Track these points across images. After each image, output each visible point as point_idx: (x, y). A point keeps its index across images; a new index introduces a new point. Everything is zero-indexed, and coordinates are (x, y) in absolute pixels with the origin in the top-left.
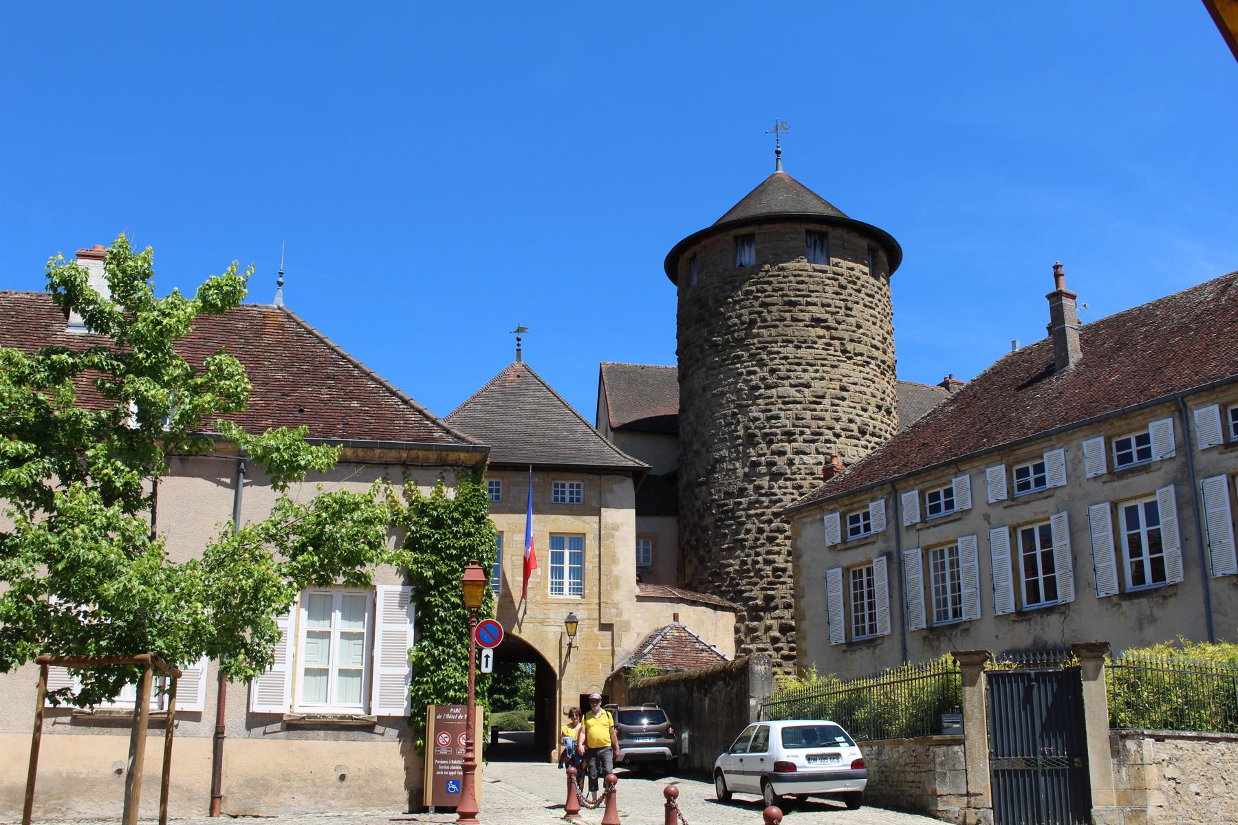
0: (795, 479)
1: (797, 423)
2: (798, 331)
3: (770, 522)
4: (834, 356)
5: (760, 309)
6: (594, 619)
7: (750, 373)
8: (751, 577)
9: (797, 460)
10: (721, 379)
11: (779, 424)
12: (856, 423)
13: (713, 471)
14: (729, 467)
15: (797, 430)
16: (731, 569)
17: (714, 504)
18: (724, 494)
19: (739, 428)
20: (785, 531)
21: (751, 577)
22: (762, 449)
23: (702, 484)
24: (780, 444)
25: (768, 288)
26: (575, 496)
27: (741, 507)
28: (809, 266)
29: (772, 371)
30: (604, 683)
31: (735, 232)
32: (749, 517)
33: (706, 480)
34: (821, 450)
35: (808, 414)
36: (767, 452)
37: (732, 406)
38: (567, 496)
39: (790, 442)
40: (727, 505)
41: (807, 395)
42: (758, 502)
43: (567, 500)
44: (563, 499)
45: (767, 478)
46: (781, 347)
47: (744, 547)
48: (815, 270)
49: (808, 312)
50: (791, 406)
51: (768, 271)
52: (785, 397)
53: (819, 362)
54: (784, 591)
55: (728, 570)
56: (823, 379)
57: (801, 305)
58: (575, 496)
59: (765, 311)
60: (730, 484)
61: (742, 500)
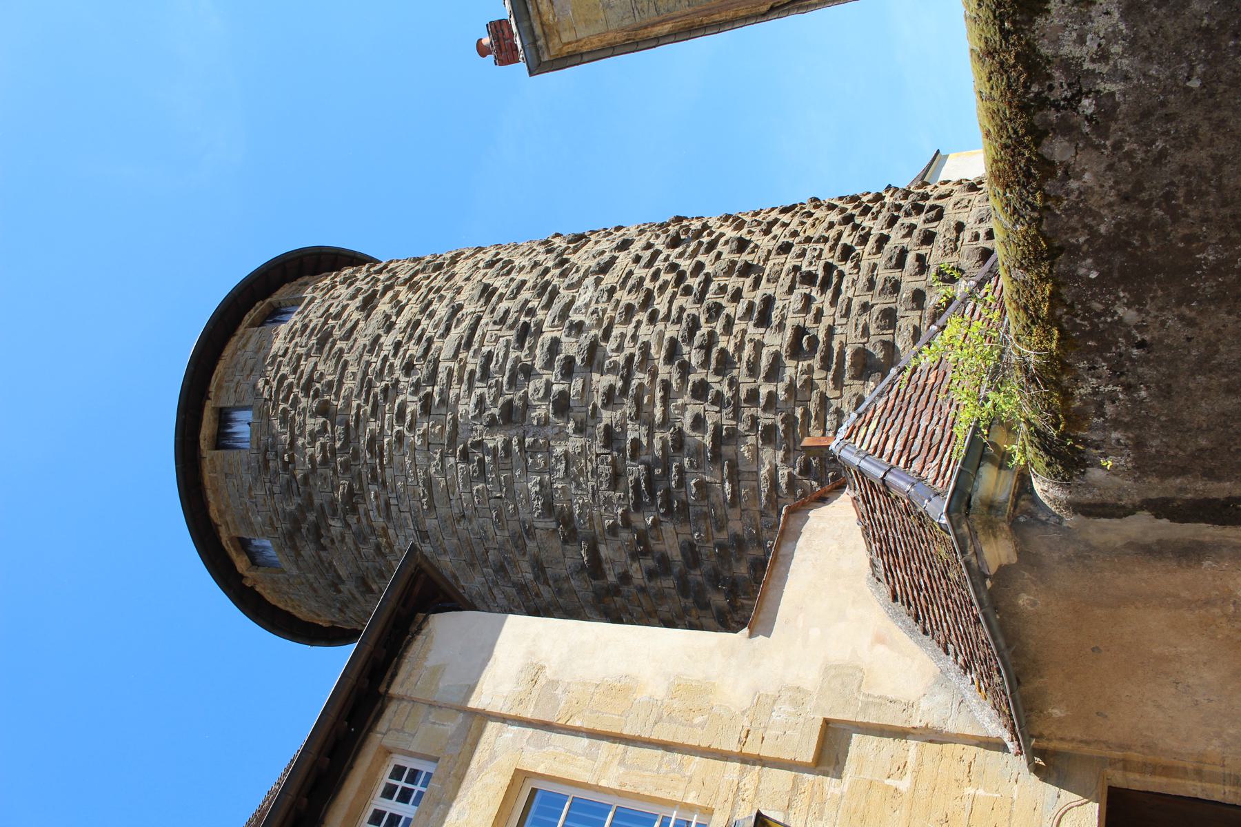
0: (612, 319)
1: (509, 321)
3: (685, 369)
4: (435, 278)
5: (312, 393)
6: (795, 787)
7: (401, 416)
8: (806, 413)
9: (575, 317)
10: (405, 486)
11: (501, 354)
13: (566, 519)
14: (561, 474)
16: (783, 472)
17: (635, 518)
18: (615, 490)
19: (491, 445)
20: (712, 334)
21: (806, 413)
22: (537, 390)
23: (593, 552)
24: (538, 352)
25: (291, 379)
27: (644, 441)
28: (294, 318)
29: (409, 368)
30: (1051, 789)
32: (666, 422)
33: (586, 540)
35: (504, 305)
36: (545, 377)
37: (452, 460)
39: (539, 332)
40: (637, 481)
41: (473, 310)
42: (638, 400)
45: (596, 376)
46: (378, 355)
47: (733, 433)
48: (302, 312)
50: (479, 332)
51: (267, 382)
52: (459, 344)
54: (850, 330)
55: (783, 482)
57: (333, 327)
59: (318, 385)
60: (594, 472)
61: (631, 435)
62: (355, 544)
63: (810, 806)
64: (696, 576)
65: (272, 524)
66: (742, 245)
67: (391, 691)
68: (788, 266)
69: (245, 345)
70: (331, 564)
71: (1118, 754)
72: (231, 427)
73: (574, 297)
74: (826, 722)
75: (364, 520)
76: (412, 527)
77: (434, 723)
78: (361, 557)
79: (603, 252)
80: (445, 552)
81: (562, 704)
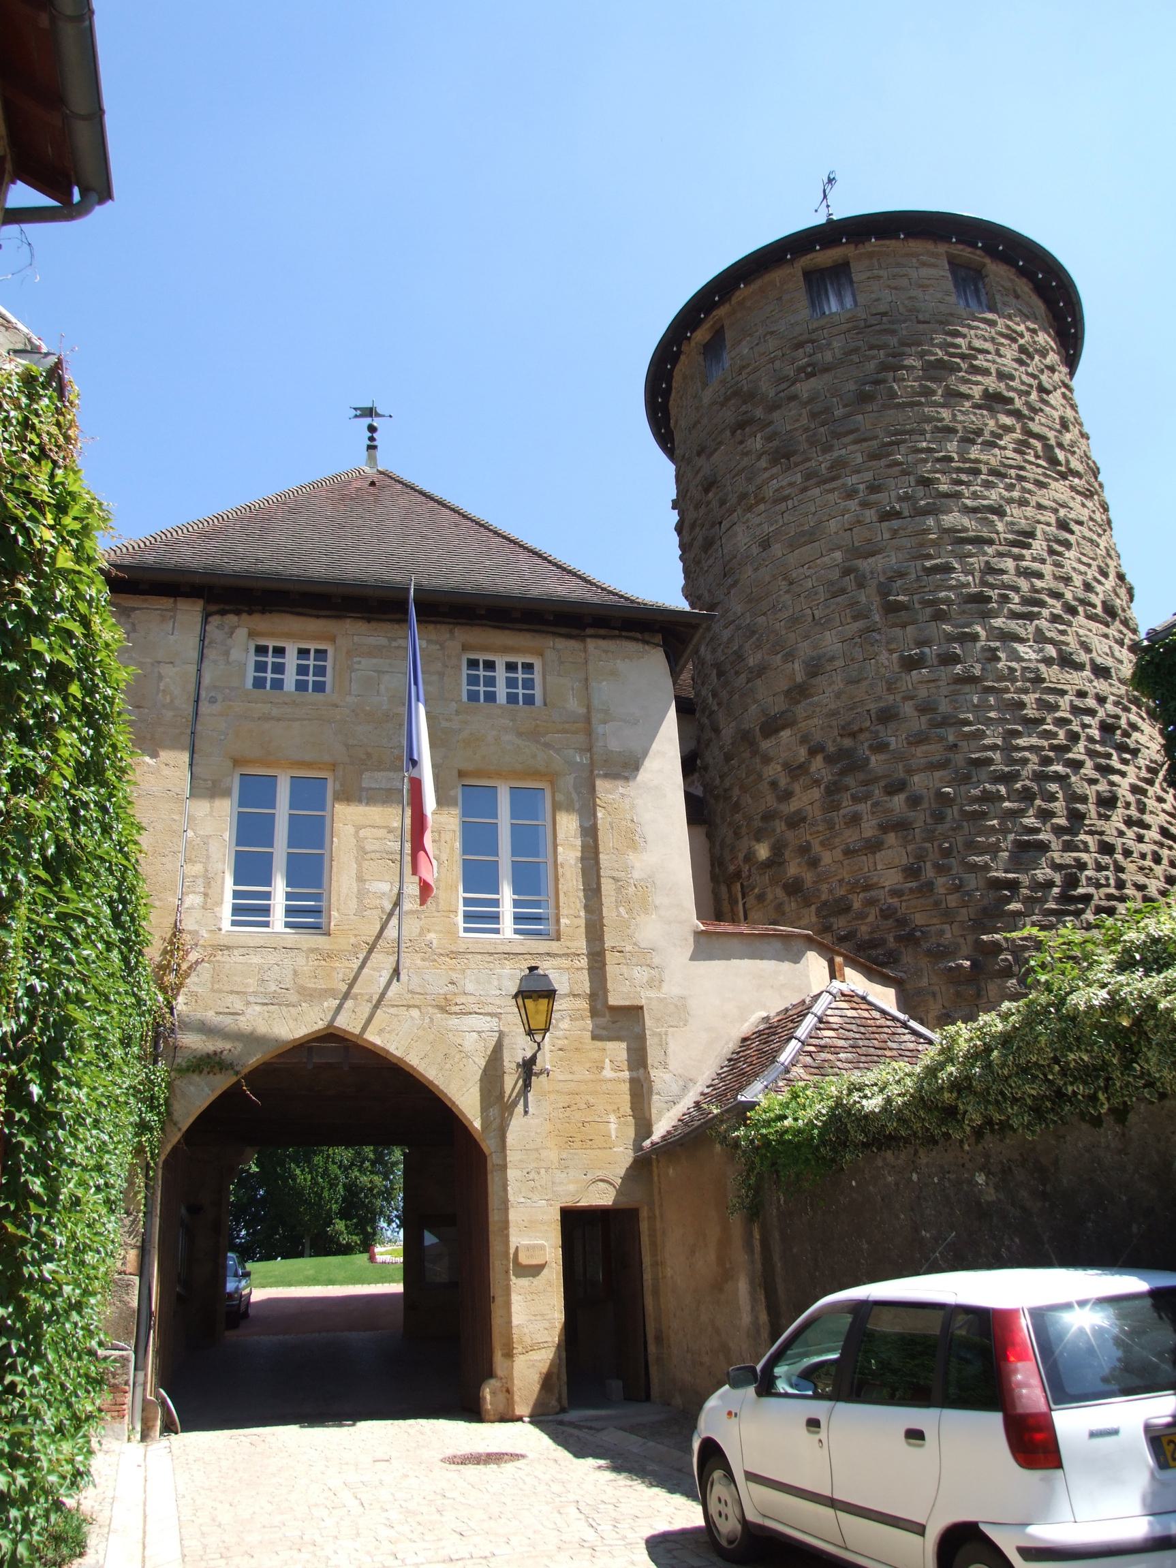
1: (990, 579)
2: (967, 416)
4: (1038, 466)
12: (1097, 594)
15: (994, 594)
25: (893, 341)
26: (520, 691)
31: (806, 261)
34: (1048, 634)
35: (1009, 564)
38: (501, 691)
43: (501, 697)
44: (491, 697)
49: (977, 383)
53: (1013, 472)
56: (1023, 503)
58: (520, 691)
62: (744, 469)
63: (578, 1010)
64: (780, 826)
65: (744, 367)
66: (1108, 802)
67: (589, 640)
68: (1084, 856)
69: (924, 264)
70: (720, 443)
71: (657, 1213)
72: (832, 284)
73: (1028, 640)
74: (641, 1008)
75: (766, 475)
76: (771, 530)
77: (573, 689)
78: (734, 477)
79: (1088, 650)
80: (756, 570)
81: (611, 797)
